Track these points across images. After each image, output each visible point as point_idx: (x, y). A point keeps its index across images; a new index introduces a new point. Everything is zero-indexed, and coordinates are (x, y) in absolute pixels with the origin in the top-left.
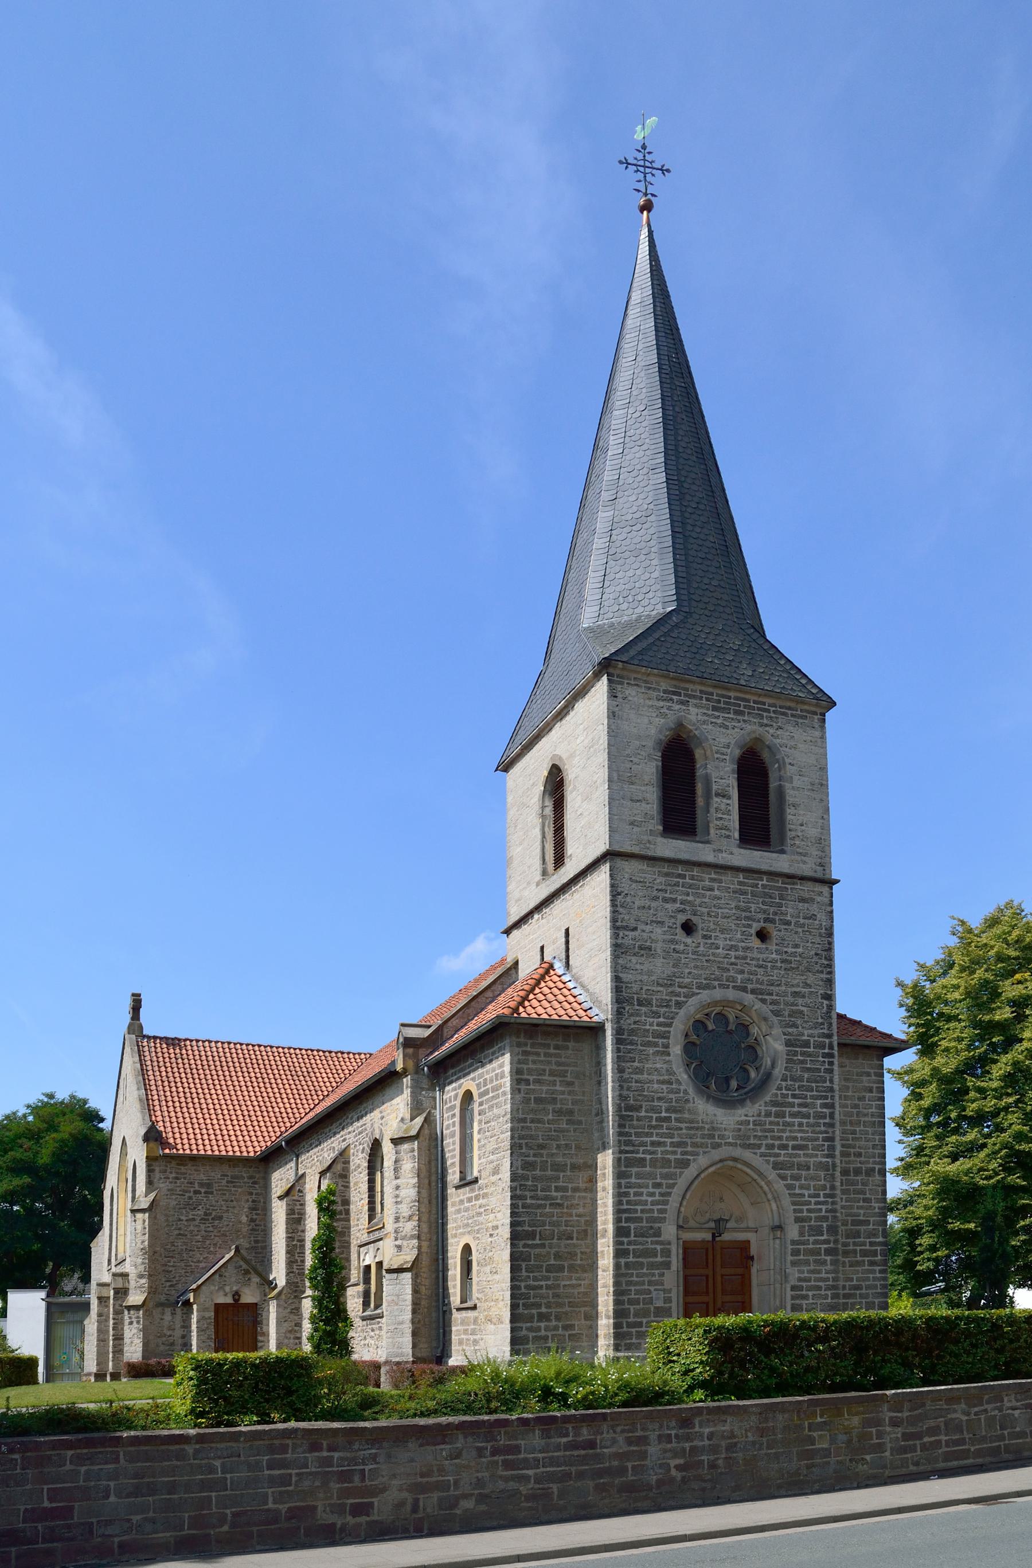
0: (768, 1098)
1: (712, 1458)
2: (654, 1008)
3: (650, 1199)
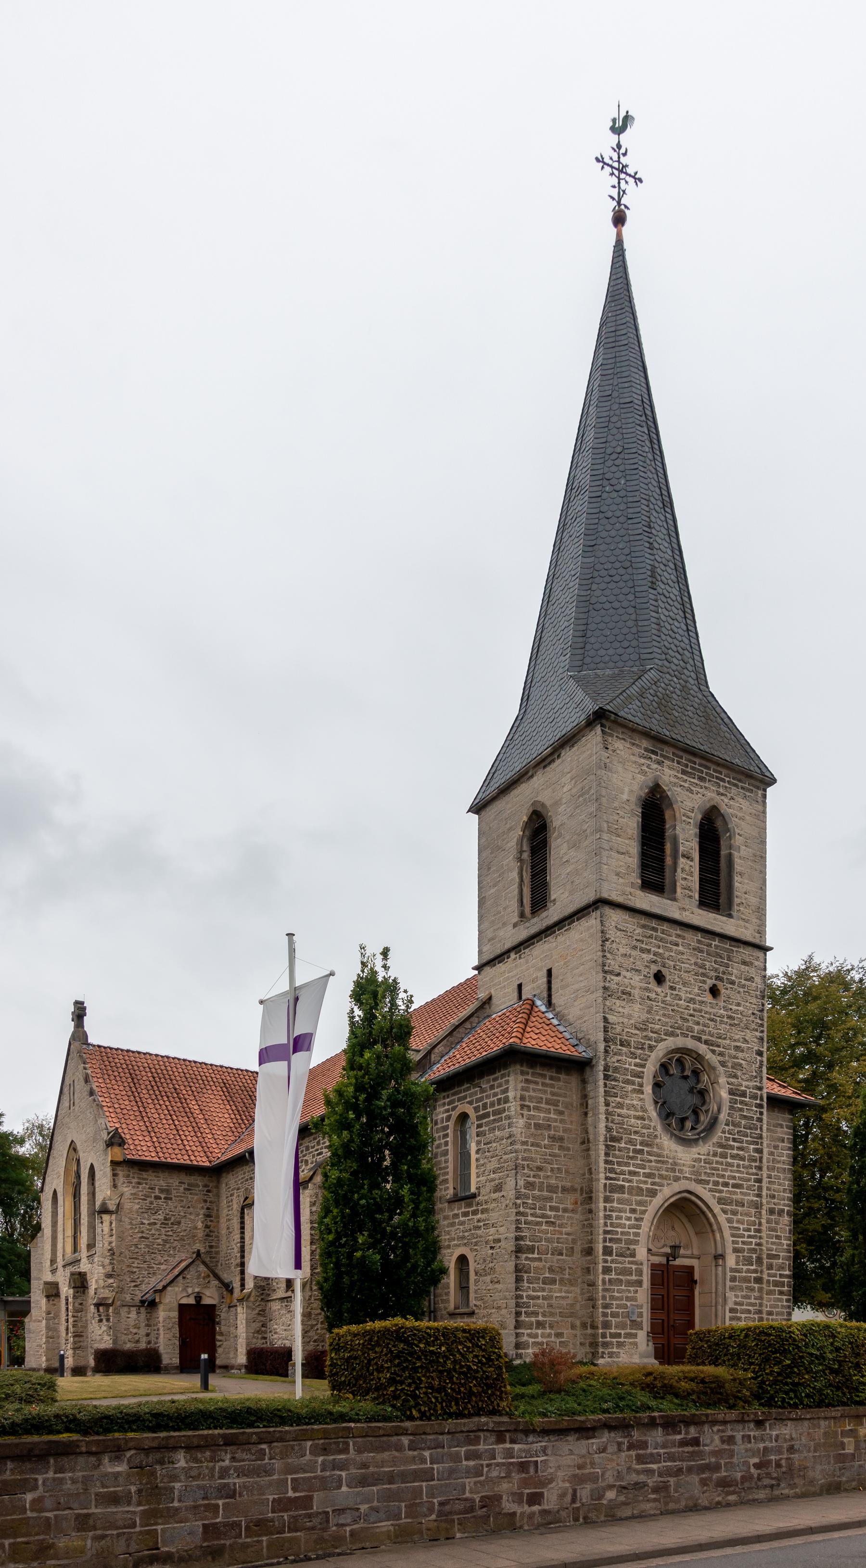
0: (715, 1140)
1: (777, 1458)
2: (632, 1050)
3: (628, 1223)
